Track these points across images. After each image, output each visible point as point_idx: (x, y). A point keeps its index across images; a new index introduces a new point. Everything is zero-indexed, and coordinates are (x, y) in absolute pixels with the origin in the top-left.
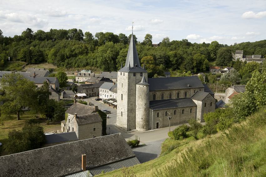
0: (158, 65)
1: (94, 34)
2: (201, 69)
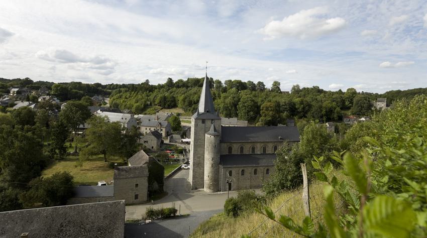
0: (282, 112)
1: (223, 82)
2: (331, 117)
